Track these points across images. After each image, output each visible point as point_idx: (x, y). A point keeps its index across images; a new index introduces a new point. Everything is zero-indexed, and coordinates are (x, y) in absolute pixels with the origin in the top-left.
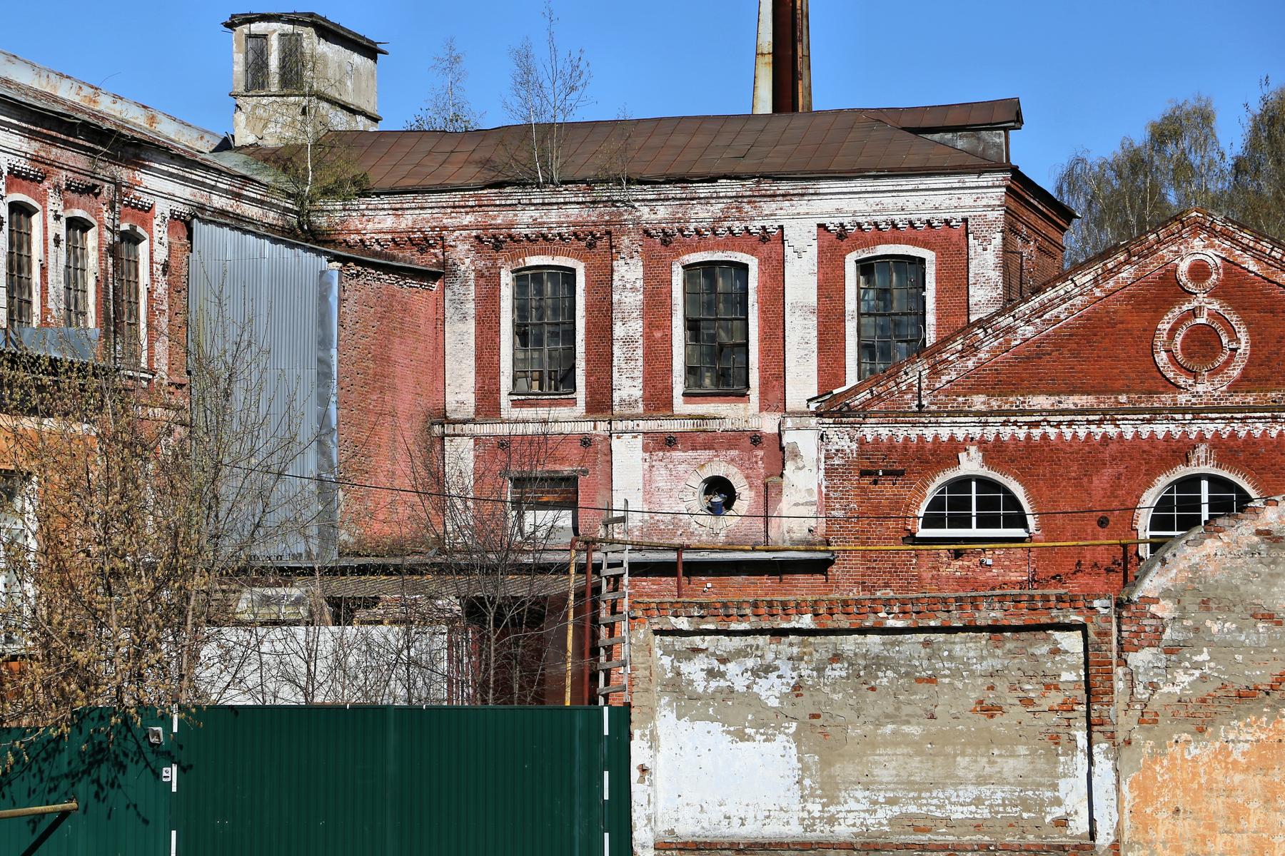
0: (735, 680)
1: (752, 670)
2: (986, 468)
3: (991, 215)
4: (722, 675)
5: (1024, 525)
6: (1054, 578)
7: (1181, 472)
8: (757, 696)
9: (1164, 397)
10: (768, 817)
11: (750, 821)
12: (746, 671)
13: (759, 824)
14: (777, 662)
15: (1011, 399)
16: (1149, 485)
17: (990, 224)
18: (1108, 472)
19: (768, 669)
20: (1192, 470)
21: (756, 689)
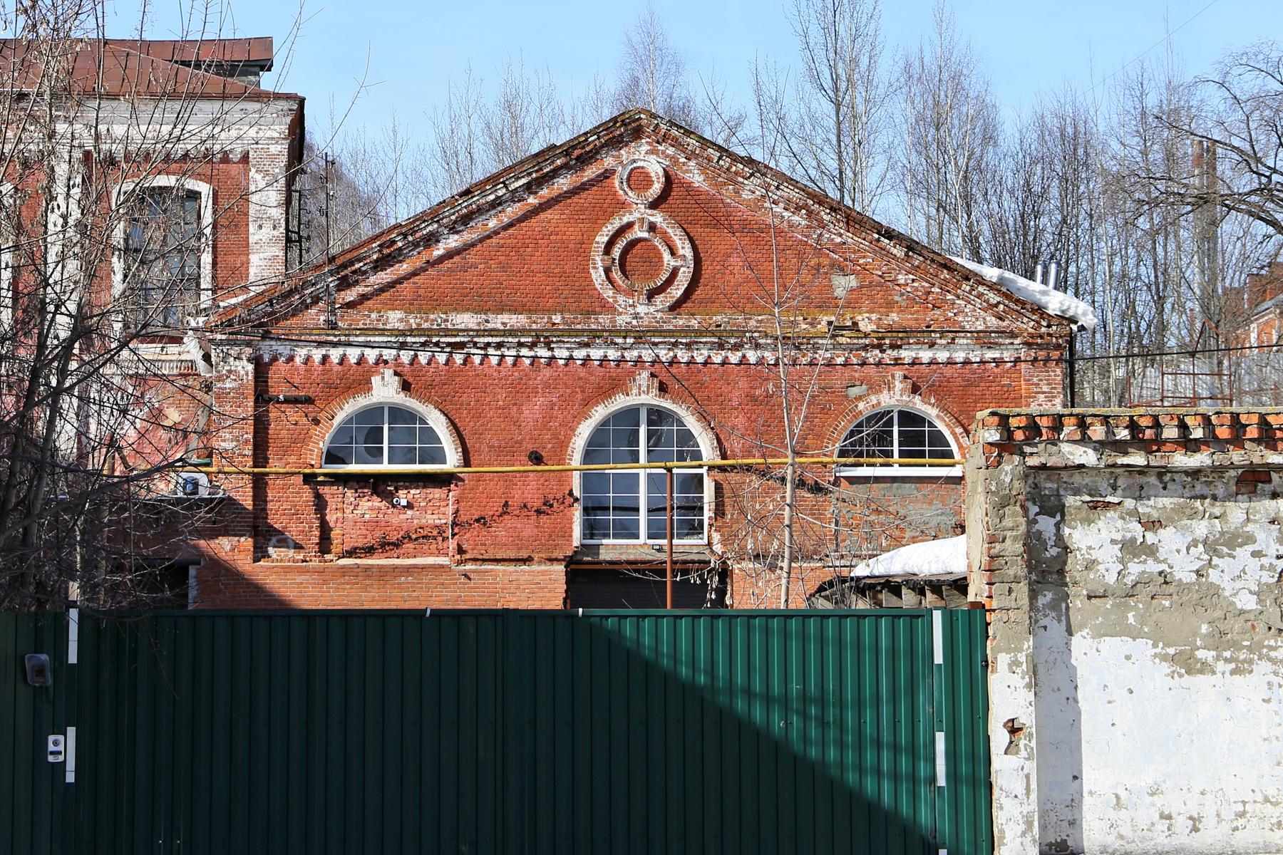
0: (1176, 560)
1: (1205, 543)
2: (402, 395)
3: (274, 149)
4: (1151, 551)
5: (439, 457)
6: (478, 521)
7: (620, 402)
8: (1215, 591)
9: (602, 318)
10: (1242, 815)
11: (1209, 823)
12: (1195, 543)
13: (1225, 827)
14: (1250, 528)
15: (432, 316)
16: (586, 416)
17: (273, 158)
18: (540, 400)
19: (1235, 540)
20: (632, 400)
21: (1213, 576)
